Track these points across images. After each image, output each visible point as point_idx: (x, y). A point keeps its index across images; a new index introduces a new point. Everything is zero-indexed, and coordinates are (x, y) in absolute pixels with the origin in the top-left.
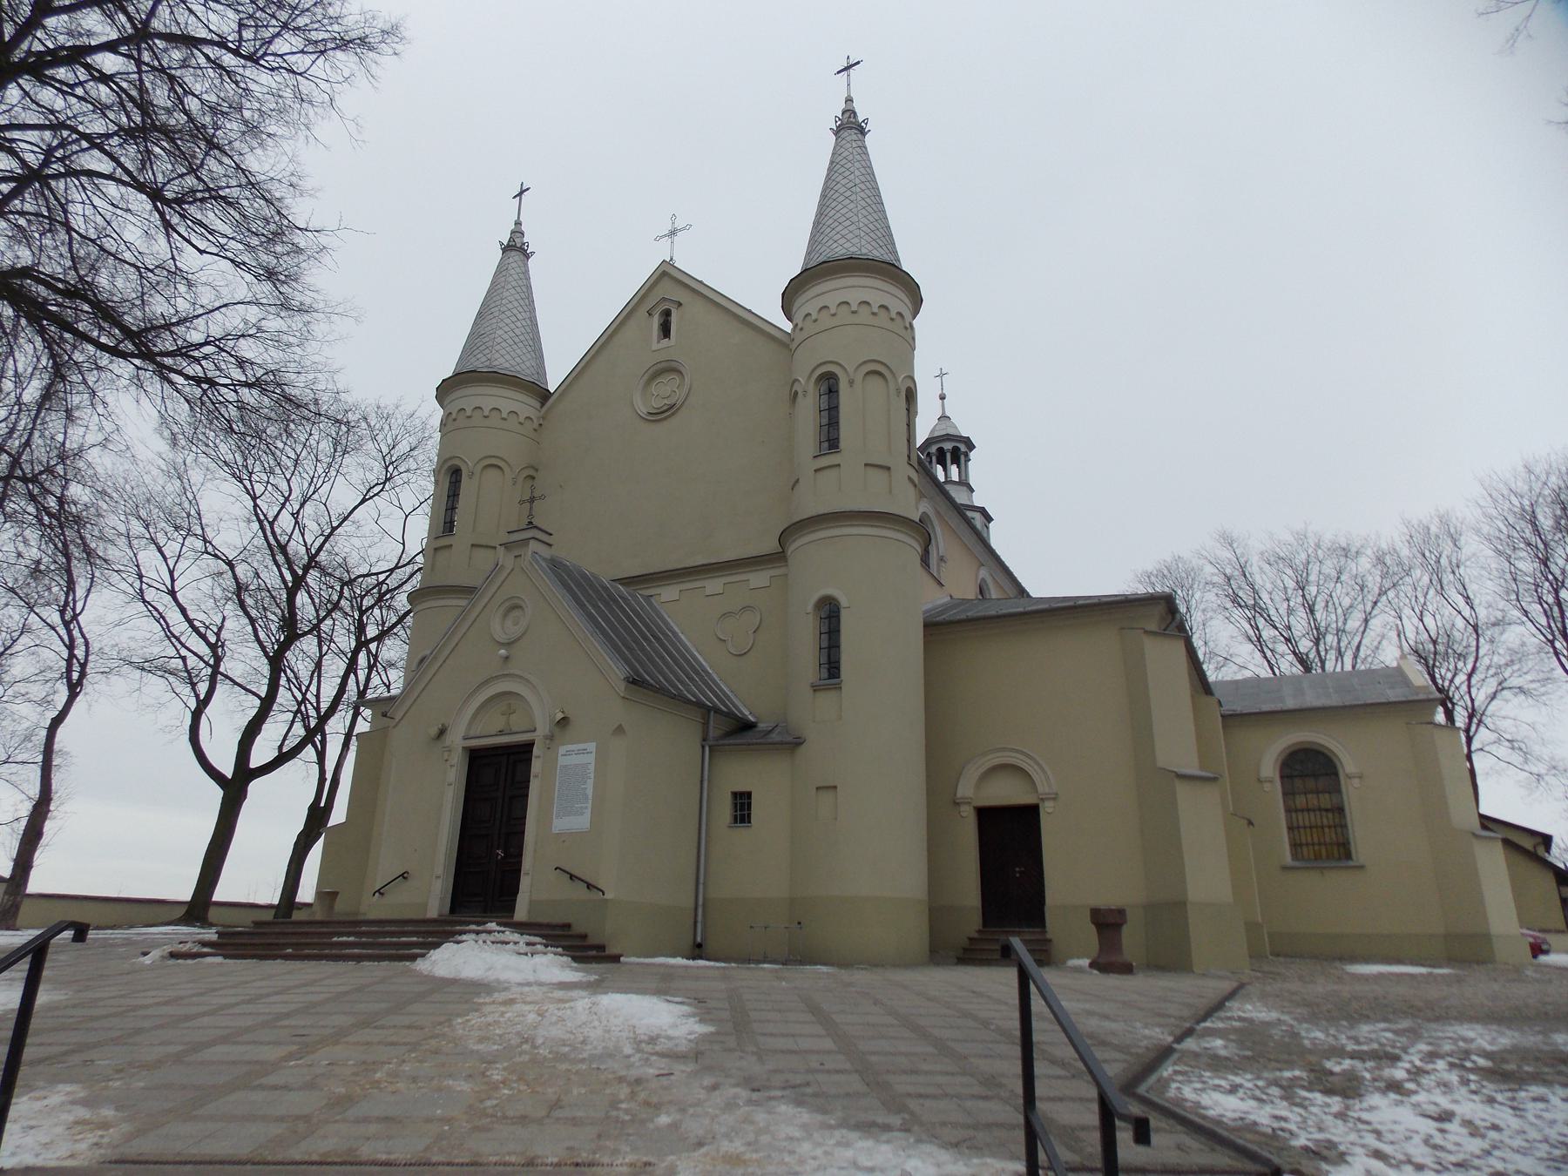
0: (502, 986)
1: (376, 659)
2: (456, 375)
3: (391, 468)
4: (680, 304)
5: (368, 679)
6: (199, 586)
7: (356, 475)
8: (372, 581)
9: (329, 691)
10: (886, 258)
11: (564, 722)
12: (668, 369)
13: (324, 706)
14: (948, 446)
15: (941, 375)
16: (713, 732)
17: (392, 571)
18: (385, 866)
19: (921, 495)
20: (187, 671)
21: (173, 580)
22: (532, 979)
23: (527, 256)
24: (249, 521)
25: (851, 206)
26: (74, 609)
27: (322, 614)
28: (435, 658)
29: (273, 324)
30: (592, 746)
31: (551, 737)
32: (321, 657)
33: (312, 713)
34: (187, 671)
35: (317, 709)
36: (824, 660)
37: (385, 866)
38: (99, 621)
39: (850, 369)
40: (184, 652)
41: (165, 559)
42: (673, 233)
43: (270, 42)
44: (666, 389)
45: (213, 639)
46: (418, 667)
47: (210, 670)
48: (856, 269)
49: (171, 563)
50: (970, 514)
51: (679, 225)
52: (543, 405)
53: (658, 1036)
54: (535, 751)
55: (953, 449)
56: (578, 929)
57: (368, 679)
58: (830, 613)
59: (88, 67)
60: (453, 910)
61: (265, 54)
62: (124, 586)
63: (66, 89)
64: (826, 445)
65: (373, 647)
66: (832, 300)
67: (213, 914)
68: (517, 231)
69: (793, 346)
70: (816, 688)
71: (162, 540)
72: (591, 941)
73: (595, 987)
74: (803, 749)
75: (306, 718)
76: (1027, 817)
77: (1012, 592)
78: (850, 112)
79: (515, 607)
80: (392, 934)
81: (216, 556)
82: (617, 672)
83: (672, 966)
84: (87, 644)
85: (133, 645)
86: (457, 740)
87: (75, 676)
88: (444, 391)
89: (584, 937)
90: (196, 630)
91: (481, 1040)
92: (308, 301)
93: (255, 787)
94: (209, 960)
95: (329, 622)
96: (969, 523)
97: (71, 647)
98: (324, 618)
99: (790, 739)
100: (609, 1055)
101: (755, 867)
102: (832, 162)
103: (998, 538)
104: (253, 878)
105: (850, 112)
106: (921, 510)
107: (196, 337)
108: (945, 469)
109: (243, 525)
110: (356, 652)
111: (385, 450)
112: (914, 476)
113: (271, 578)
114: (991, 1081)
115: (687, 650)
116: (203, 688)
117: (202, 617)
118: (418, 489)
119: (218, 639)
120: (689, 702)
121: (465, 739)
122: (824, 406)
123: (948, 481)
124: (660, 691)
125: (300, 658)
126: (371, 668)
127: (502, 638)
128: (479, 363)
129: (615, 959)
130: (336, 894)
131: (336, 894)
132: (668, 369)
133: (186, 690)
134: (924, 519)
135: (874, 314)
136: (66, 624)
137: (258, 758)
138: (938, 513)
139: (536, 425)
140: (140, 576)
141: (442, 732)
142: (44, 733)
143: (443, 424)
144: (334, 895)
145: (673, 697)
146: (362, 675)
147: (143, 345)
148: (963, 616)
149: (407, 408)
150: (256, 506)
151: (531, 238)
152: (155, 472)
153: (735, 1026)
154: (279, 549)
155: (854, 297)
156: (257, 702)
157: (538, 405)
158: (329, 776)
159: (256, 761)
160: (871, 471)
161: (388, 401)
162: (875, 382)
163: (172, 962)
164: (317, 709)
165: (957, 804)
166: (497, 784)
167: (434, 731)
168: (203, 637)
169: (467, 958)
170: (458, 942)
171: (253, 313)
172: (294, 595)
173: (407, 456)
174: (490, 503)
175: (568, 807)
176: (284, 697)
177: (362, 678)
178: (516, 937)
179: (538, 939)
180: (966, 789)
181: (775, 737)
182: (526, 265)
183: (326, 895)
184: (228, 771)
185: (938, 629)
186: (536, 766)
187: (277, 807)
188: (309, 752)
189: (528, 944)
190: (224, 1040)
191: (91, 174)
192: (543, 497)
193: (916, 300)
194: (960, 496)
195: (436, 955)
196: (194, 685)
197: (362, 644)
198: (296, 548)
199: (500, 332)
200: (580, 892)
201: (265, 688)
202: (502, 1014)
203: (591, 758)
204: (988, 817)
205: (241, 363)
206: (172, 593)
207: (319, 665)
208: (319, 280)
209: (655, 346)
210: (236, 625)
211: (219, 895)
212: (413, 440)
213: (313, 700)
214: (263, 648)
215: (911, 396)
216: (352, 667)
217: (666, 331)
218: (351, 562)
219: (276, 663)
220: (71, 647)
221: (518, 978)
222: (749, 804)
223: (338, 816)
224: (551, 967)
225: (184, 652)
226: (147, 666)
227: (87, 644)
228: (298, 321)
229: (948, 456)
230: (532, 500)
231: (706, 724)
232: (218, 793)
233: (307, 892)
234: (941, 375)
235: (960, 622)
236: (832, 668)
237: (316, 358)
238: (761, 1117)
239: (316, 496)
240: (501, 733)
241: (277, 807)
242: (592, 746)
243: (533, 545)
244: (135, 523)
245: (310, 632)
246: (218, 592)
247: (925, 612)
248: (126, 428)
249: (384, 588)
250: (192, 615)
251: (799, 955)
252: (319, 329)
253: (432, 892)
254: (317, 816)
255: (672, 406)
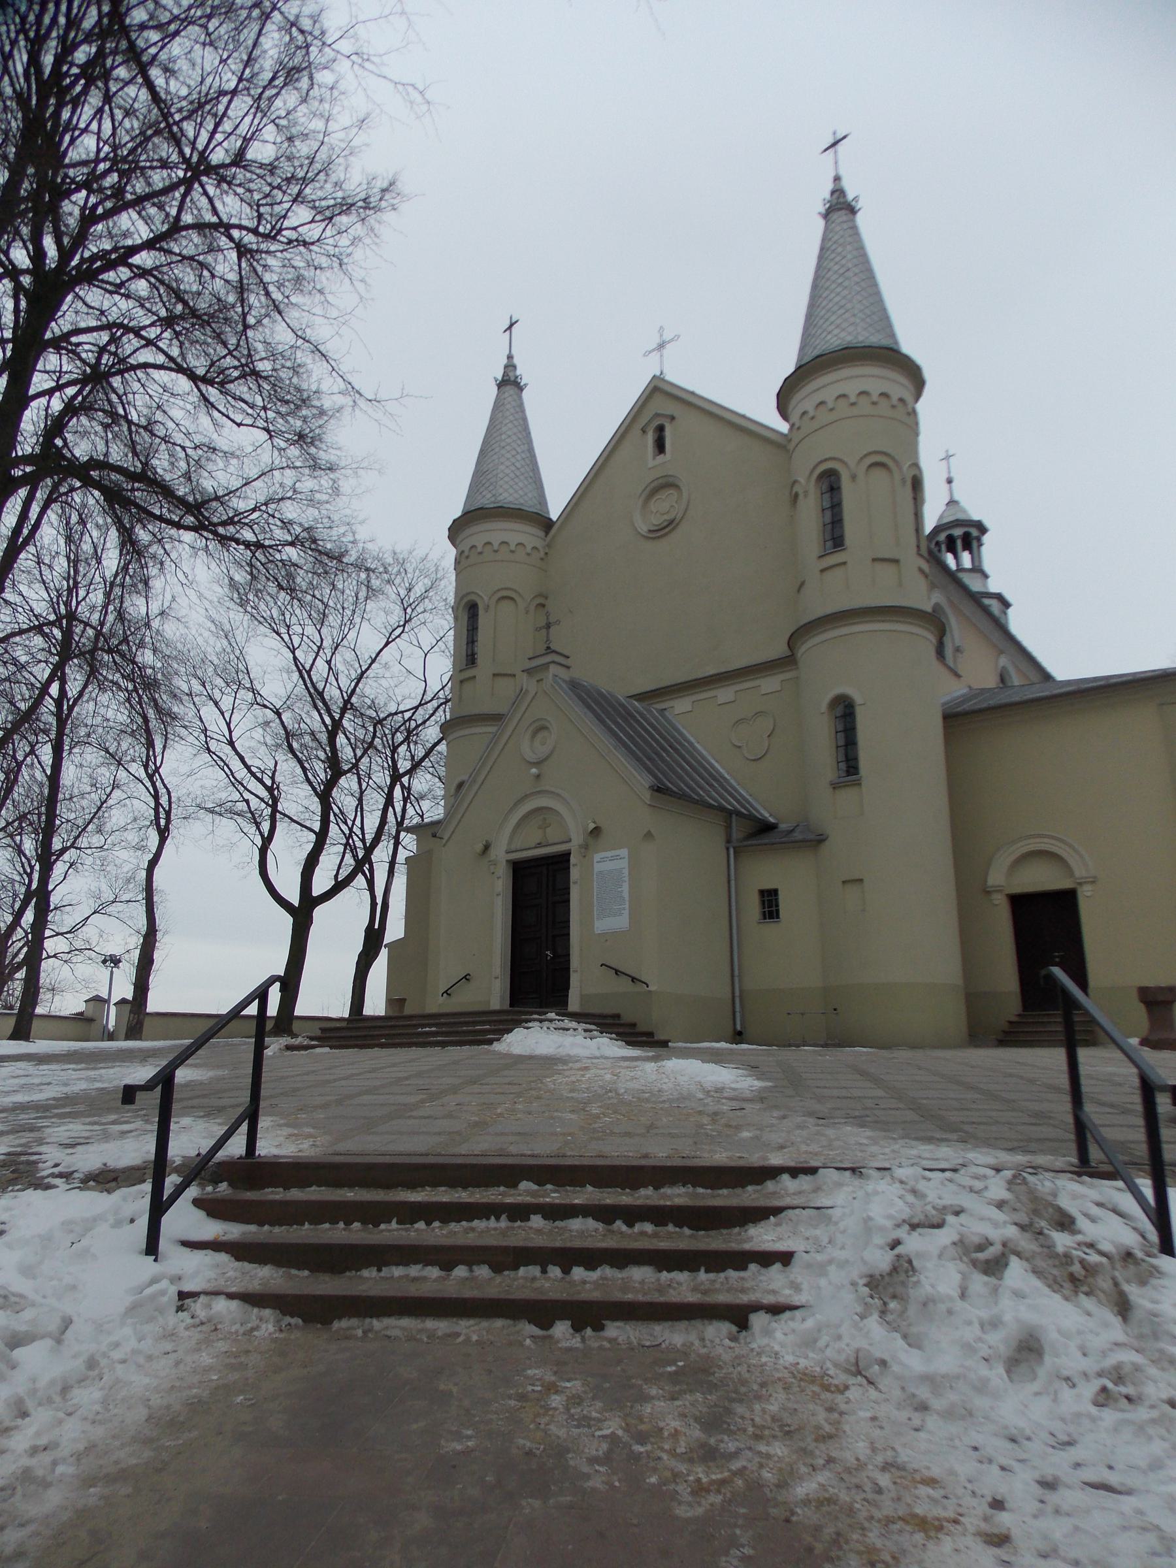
0: (578, 1060)
1: (409, 793)
2: (466, 514)
3: (409, 610)
4: (673, 418)
5: (404, 810)
6: (253, 736)
7: (379, 619)
8: (399, 718)
9: (371, 823)
10: (885, 342)
11: (596, 832)
12: (667, 484)
13: (369, 838)
14: (958, 532)
15: (947, 457)
16: (736, 835)
17: (416, 708)
18: (445, 972)
19: (933, 586)
20: (251, 812)
21: (230, 732)
22: (597, 1054)
23: (521, 389)
24: (288, 672)
25: (846, 292)
26: (155, 764)
27: (359, 753)
28: (474, 781)
29: (307, 484)
30: (624, 852)
31: (585, 846)
32: (362, 793)
33: (359, 844)
34: (251, 812)
35: (363, 840)
36: (842, 757)
37: (445, 972)
38: (174, 773)
39: (486, 598)
40: (247, 795)
41: (222, 714)
42: (661, 346)
43: (285, 217)
44: (664, 505)
45: (269, 782)
46: (457, 791)
47: (270, 810)
48: (856, 361)
49: (227, 716)
50: (986, 601)
51: (666, 337)
52: (547, 533)
53: (723, 1088)
54: (573, 860)
55: (965, 535)
56: (627, 1018)
57: (404, 810)
58: (845, 711)
59: (130, 266)
60: (512, 1004)
61: (281, 230)
62: (191, 739)
63: (118, 288)
64: (829, 544)
65: (405, 780)
66: (829, 395)
67: (296, 1026)
68: (510, 366)
69: (791, 447)
70: (835, 786)
71: (217, 695)
72: (642, 1028)
73: (655, 1059)
74: (827, 843)
75: (354, 850)
76: (775, 892)
77: (1034, 676)
78: (838, 192)
79: (541, 728)
80: (467, 1023)
81: (265, 706)
82: (642, 781)
83: (718, 1049)
84: (169, 793)
85: (205, 792)
86: (501, 853)
87: (163, 822)
88: (456, 531)
89: (634, 1025)
90: (253, 774)
91: (572, 1091)
92: (333, 458)
93: (319, 912)
94: (318, 1050)
95: (365, 760)
96: (986, 611)
97: (156, 797)
98: (361, 757)
99: (812, 837)
100: (682, 1098)
101: (787, 959)
102: (822, 249)
103: (1018, 623)
104: (324, 994)
105: (838, 192)
106: (933, 601)
107: (242, 505)
108: (956, 557)
109: (285, 675)
110: (391, 789)
111: (403, 593)
112: (925, 566)
113: (314, 721)
114: (1041, 1117)
115: (703, 757)
116: (266, 827)
117: (257, 763)
118: (438, 626)
119: (273, 782)
120: (710, 806)
121: (508, 852)
122: (827, 504)
123: (960, 569)
124: (682, 797)
125: (344, 795)
126: (405, 800)
127: (530, 756)
128: (486, 500)
129: (664, 1044)
130: (405, 1000)
131: (405, 1000)
132: (667, 484)
133: (252, 829)
134: (937, 607)
135: (874, 403)
136: (150, 777)
137: (318, 888)
138: (951, 603)
139: (542, 554)
140: (205, 731)
141: (487, 847)
142: (144, 874)
143: (457, 562)
144: (402, 1001)
145: (696, 802)
146: (398, 807)
147: (201, 515)
148: (985, 705)
149: (419, 553)
150: (295, 658)
151: (523, 371)
152: (206, 634)
153: (793, 1082)
154: (317, 696)
155: (851, 389)
156: (313, 837)
157: (542, 534)
158: (379, 901)
159: (317, 891)
160: (879, 566)
161: (402, 548)
162: (879, 475)
163: (289, 1053)
164: (363, 840)
165: (988, 893)
166: (540, 892)
167: (479, 847)
168: (261, 781)
169: (532, 1040)
170: (528, 1028)
171: (289, 476)
172: (336, 737)
173: (423, 598)
174: (506, 631)
175: (607, 909)
176: (333, 829)
177: (399, 809)
178: (574, 1024)
179: (593, 1027)
180: (996, 877)
181: (797, 836)
182: (520, 398)
183: (393, 1001)
184: (295, 901)
185: (958, 721)
186: (574, 873)
187: (340, 926)
188: (360, 881)
189: (585, 1031)
190: (368, 1092)
191: (145, 366)
192: (558, 622)
193: (914, 376)
194: (975, 584)
195: (509, 1038)
196: (258, 825)
197: (396, 777)
198: (332, 693)
199: (502, 467)
200: (624, 985)
201: (318, 823)
202: (583, 1076)
203: (624, 864)
204: (1020, 903)
205: (286, 524)
206: (231, 743)
207: (360, 800)
208: (346, 437)
209: (651, 463)
210: (288, 769)
211: (299, 1011)
212: (428, 582)
213: (359, 832)
214: (314, 789)
215: (917, 484)
216: (389, 801)
217: (660, 446)
218: (380, 701)
219: (325, 797)
220: (156, 797)
221: (586, 1053)
222: (777, 900)
223: (395, 930)
224: (608, 1047)
225: (247, 795)
226: (219, 810)
227: (169, 793)
228: (325, 482)
229: (959, 543)
230: (548, 626)
231: (728, 827)
232: (289, 920)
233: (375, 1004)
234: (947, 457)
235: (981, 711)
236: (850, 765)
237: (348, 512)
238: (831, 1132)
239: (345, 642)
240: (539, 845)
241: (340, 926)
242: (624, 852)
243: (553, 669)
244: (194, 682)
245: (349, 771)
246: (269, 740)
247: (944, 704)
248: (190, 594)
249: (413, 724)
250: (249, 763)
251: (836, 1040)
252: (346, 486)
253: (492, 989)
254: (373, 938)
255: (671, 522)
